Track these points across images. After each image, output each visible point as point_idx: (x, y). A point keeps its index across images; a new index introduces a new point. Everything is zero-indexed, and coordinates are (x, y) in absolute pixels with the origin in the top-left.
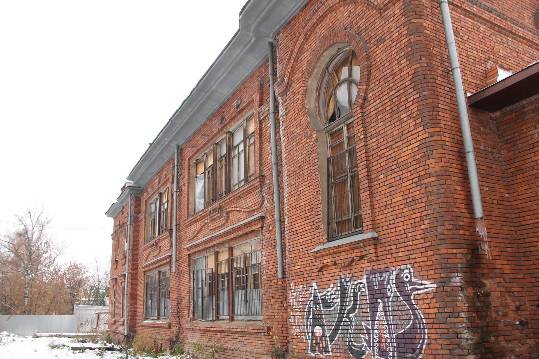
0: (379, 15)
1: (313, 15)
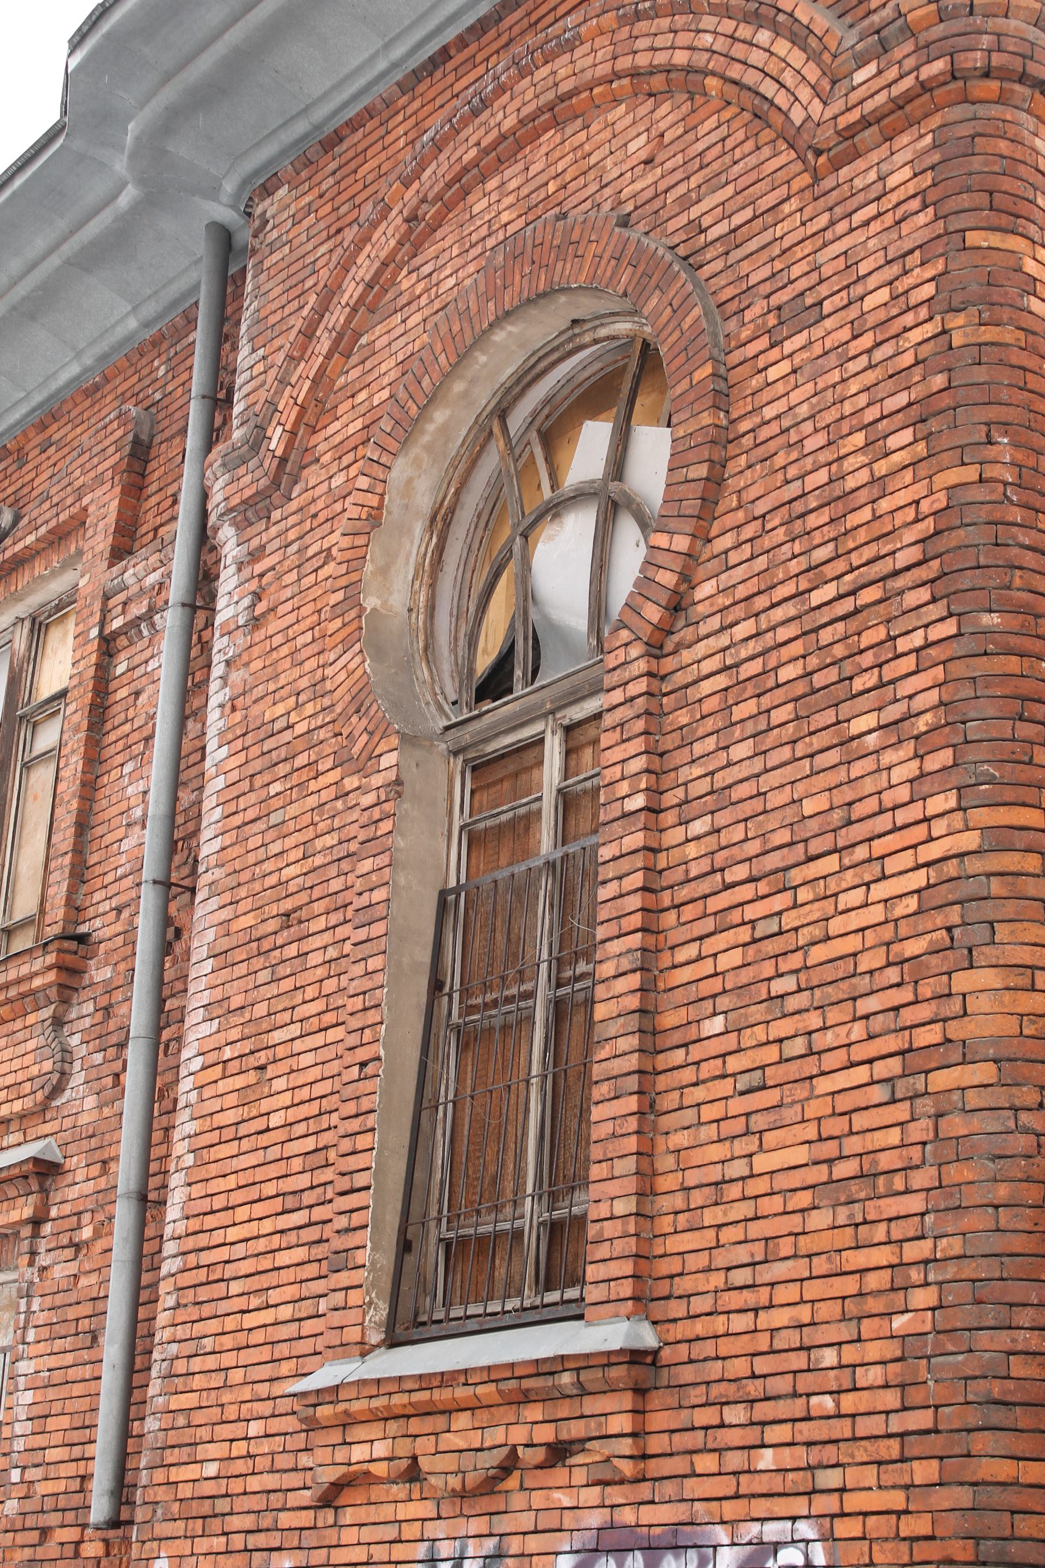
0: (806, 179)
1: (465, 122)
